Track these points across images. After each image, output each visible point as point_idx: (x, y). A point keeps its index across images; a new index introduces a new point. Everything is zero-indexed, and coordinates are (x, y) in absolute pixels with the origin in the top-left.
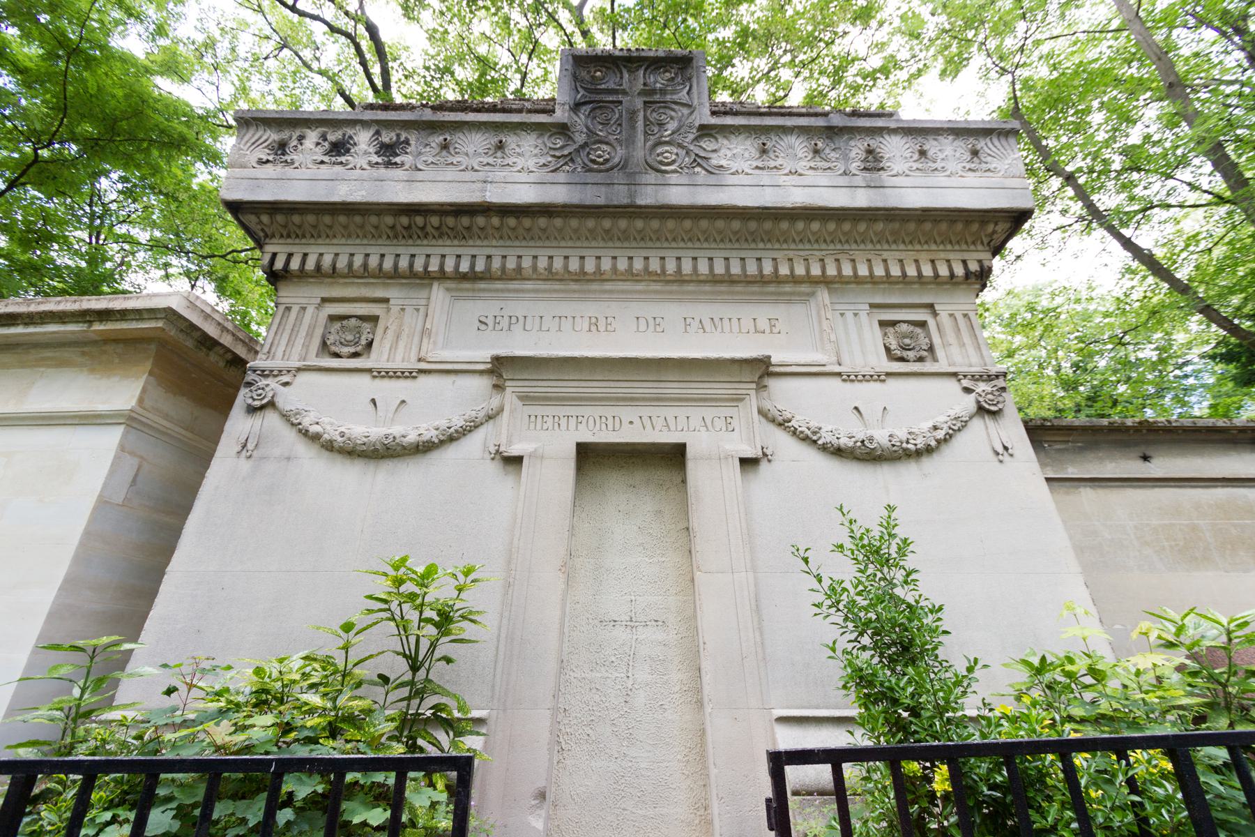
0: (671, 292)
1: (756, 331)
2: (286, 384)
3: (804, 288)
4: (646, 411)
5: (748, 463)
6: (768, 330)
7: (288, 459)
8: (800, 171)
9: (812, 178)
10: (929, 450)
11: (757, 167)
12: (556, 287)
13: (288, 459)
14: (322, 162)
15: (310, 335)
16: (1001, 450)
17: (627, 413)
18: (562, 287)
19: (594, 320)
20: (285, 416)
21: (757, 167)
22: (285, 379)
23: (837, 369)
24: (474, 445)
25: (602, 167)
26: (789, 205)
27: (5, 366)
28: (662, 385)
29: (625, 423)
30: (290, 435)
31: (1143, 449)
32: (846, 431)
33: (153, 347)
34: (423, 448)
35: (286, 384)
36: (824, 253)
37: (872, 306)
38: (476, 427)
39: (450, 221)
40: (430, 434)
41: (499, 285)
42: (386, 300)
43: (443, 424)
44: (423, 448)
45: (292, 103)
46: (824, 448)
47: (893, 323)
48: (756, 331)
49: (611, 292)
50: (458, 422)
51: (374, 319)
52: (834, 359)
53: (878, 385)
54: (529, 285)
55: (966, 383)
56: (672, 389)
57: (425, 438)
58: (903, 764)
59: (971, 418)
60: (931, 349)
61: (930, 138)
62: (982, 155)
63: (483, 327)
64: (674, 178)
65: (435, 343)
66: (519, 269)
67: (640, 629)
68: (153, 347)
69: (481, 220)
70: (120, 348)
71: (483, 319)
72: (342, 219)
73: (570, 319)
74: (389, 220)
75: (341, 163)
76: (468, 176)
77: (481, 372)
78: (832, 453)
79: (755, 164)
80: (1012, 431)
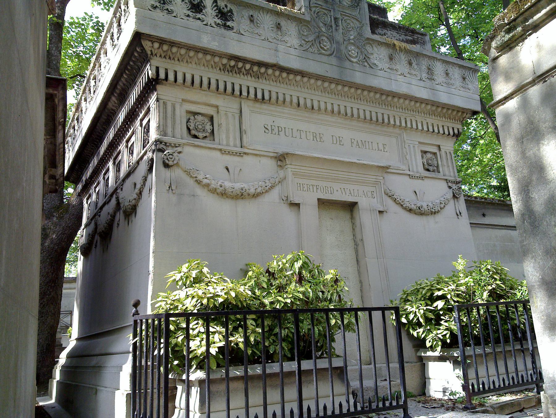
1: (378, 150)
5: (380, 212)
6: (383, 150)
8: (405, 74)
16: (459, 214)
18: (307, 115)
19: (315, 135)
20: (188, 173)
23: (409, 173)
24: (275, 194)
29: (335, 191)
30: (191, 182)
31: (483, 211)
32: (410, 200)
36: (406, 115)
37: (420, 143)
39: (255, 68)
45: (501, 90)
46: (405, 209)
48: (378, 150)
55: (450, 184)
60: (437, 167)
61: (451, 66)
62: (466, 80)
63: (267, 131)
64: (381, 73)
70: (358, 230)
71: (266, 126)
72: (200, 55)
73: (305, 132)
75: (199, 19)
76: (266, 43)
77: (271, 157)
78: (408, 211)
80: (462, 205)
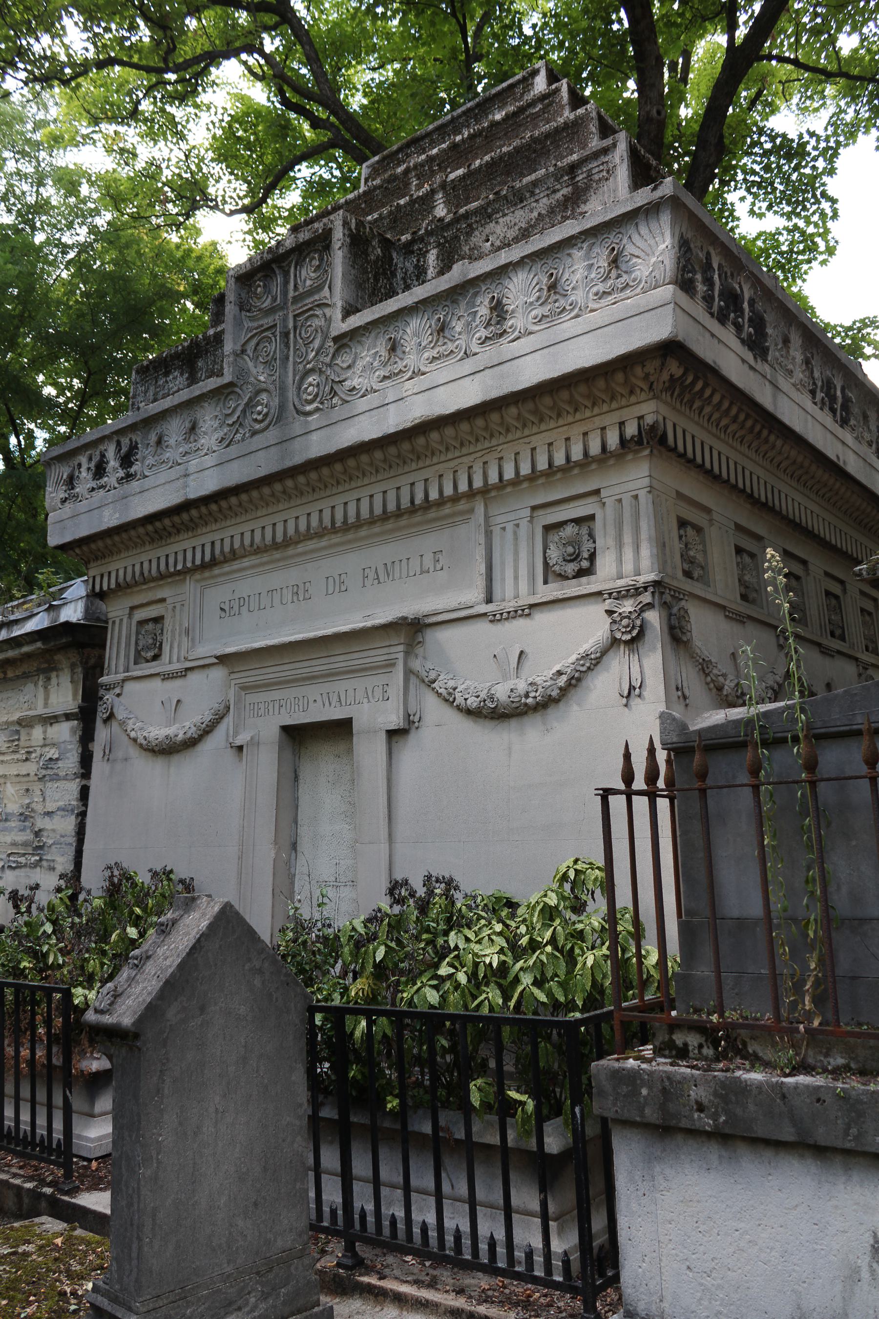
0: (349, 542)
2: (118, 695)
3: (462, 506)
4: (325, 688)
7: (126, 759)
9: (441, 373)
10: (556, 701)
11: (385, 378)
12: (265, 559)
13: (126, 759)
14: (93, 489)
15: (128, 645)
17: (313, 691)
21: (385, 378)
22: (117, 691)
25: (266, 422)
26: (409, 425)
27: (5, 695)
28: (332, 659)
29: (311, 701)
33: (666, 218)
34: (191, 743)
35: (118, 695)
38: (222, 718)
40: (193, 732)
41: (227, 568)
42: (163, 600)
43: (197, 719)
44: (191, 743)
47: (559, 525)
49: (305, 553)
50: (208, 717)
51: (158, 620)
52: (482, 596)
53: (521, 622)
54: (246, 562)
56: (340, 662)
57: (189, 735)
58: (336, 1117)
59: (604, 652)
63: (223, 614)
65: (193, 640)
66: (233, 551)
67: (342, 888)
68: (666, 218)
69: (194, 513)
74: (141, 530)
79: (381, 373)
